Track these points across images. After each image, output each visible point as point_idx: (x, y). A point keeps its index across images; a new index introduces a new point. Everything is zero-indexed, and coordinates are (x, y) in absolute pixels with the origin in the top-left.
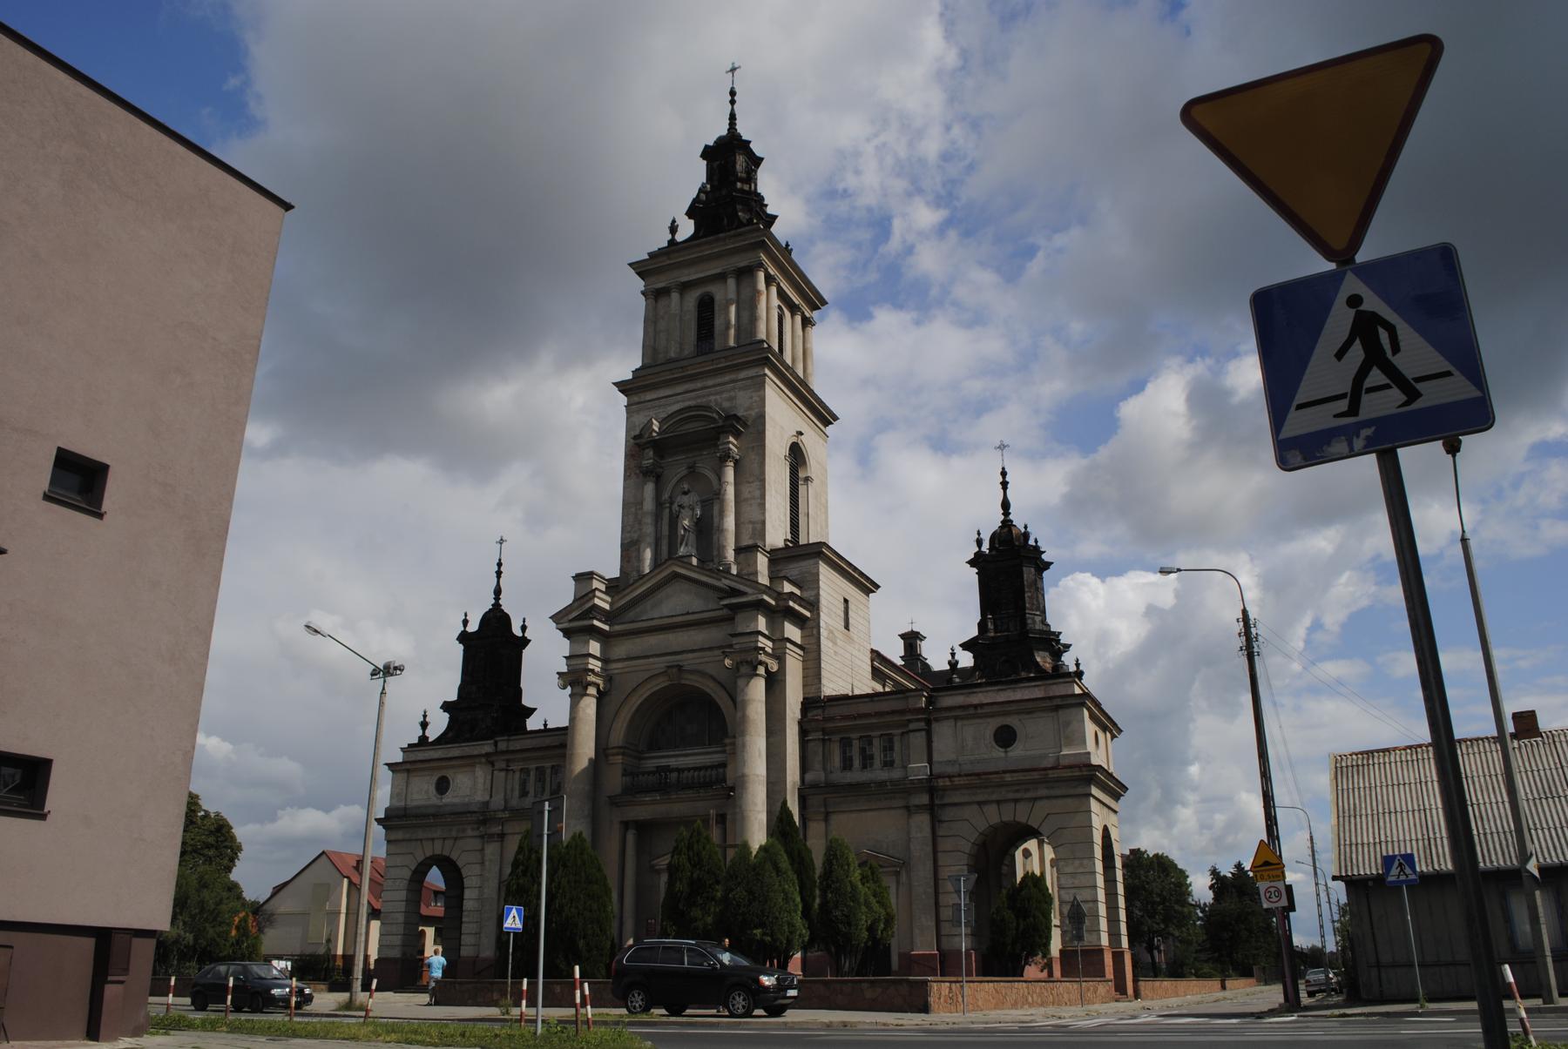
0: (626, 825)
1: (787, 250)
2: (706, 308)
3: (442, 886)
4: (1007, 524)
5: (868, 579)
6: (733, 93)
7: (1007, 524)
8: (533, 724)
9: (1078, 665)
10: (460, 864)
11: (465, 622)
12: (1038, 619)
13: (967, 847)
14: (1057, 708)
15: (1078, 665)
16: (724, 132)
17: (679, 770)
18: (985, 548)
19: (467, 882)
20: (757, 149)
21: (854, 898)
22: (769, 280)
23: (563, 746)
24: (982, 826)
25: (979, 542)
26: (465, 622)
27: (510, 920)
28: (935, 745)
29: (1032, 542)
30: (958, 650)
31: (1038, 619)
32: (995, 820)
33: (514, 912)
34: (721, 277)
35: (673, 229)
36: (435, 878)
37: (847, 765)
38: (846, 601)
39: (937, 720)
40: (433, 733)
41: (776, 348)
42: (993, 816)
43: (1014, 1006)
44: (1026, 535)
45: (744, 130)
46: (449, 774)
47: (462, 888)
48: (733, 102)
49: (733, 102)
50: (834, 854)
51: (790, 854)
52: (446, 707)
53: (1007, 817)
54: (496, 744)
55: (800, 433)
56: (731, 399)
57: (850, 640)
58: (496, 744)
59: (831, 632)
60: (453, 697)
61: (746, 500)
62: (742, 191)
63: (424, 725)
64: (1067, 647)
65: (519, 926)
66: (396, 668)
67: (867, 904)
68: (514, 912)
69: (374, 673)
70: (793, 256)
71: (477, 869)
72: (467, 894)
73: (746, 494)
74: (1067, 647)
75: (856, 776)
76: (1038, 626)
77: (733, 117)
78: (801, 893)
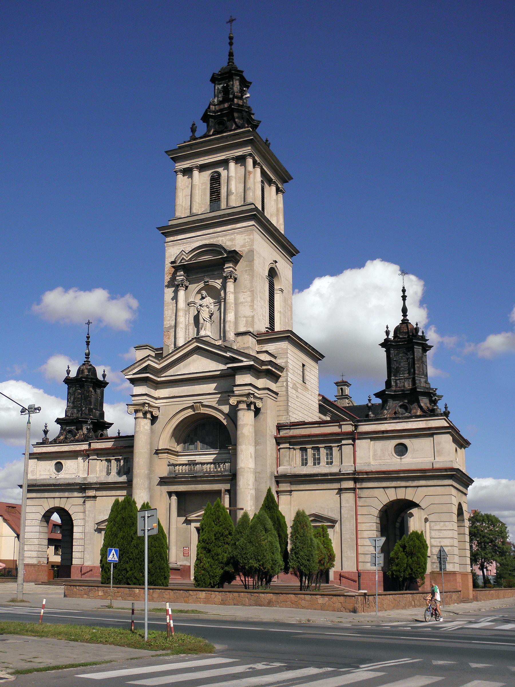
0: (170, 494)
1: (267, 143)
2: (215, 180)
3: (59, 521)
4: (405, 322)
5: (317, 352)
6: (231, 38)
7: (405, 322)
8: (111, 432)
9: (446, 408)
10: (70, 512)
11: (68, 372)
12: (423, 380)
13: (376, 513)
14: (432, 435)
15: (446, 408)
16: (225, 64)
17: (203, 464)
18: (391, 336)
19: (75, 523)
20: (247, 77)
21: (312, 545)
22: (255, 163)
23: (132, 447)
24: (386, 501)
25: (387, 333)
26: (68, 372)
27: (111, 556)
28: (357, 454)
29: (420, 334)
30: (373, 398)
31: (423, 380)
32: (393, 498)
33: (113, 551)
34: (225, 163)
35: (193, 129)
36: (56, 518)
37: (304, 462)
38: (304, 365)
39: (359, 439)
40: (51, 437)
41: (260, 208)
42: (392, 495)
43: (404, 608)
44: (417, 330)
45: (239, 64)
46: (63, 461)
47: (72, 526)
48: (231, 44)
49: (231, 44)
50: (300, 517)
51: (272, 518)
52: (59, 421)
53: (401, 496)
54: (90, 445)
55: (276, 262)
56: (232, 240)
57: (306, 389)
58: (90, 445)
59: (294, 384)
60: (63, 416)
61: (242, 303)
62: (239, 105)
63: (46, 432)
64: (440, 397)
65: (117, 559)
66: (36, 409)
67: (319, 547)
68: (113, 551)
69: (23, 411)
70: (271, 147)
71: (81, 516)
72: (75, 529)
73: (241, 300)
74: (440, 397)
75: (310, 469)
76: (423, 385)
77: (231, 54)
78: (280, 544)
